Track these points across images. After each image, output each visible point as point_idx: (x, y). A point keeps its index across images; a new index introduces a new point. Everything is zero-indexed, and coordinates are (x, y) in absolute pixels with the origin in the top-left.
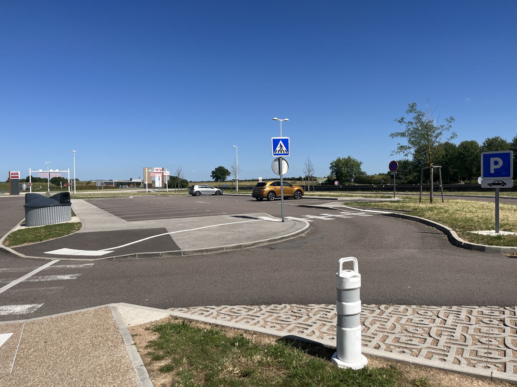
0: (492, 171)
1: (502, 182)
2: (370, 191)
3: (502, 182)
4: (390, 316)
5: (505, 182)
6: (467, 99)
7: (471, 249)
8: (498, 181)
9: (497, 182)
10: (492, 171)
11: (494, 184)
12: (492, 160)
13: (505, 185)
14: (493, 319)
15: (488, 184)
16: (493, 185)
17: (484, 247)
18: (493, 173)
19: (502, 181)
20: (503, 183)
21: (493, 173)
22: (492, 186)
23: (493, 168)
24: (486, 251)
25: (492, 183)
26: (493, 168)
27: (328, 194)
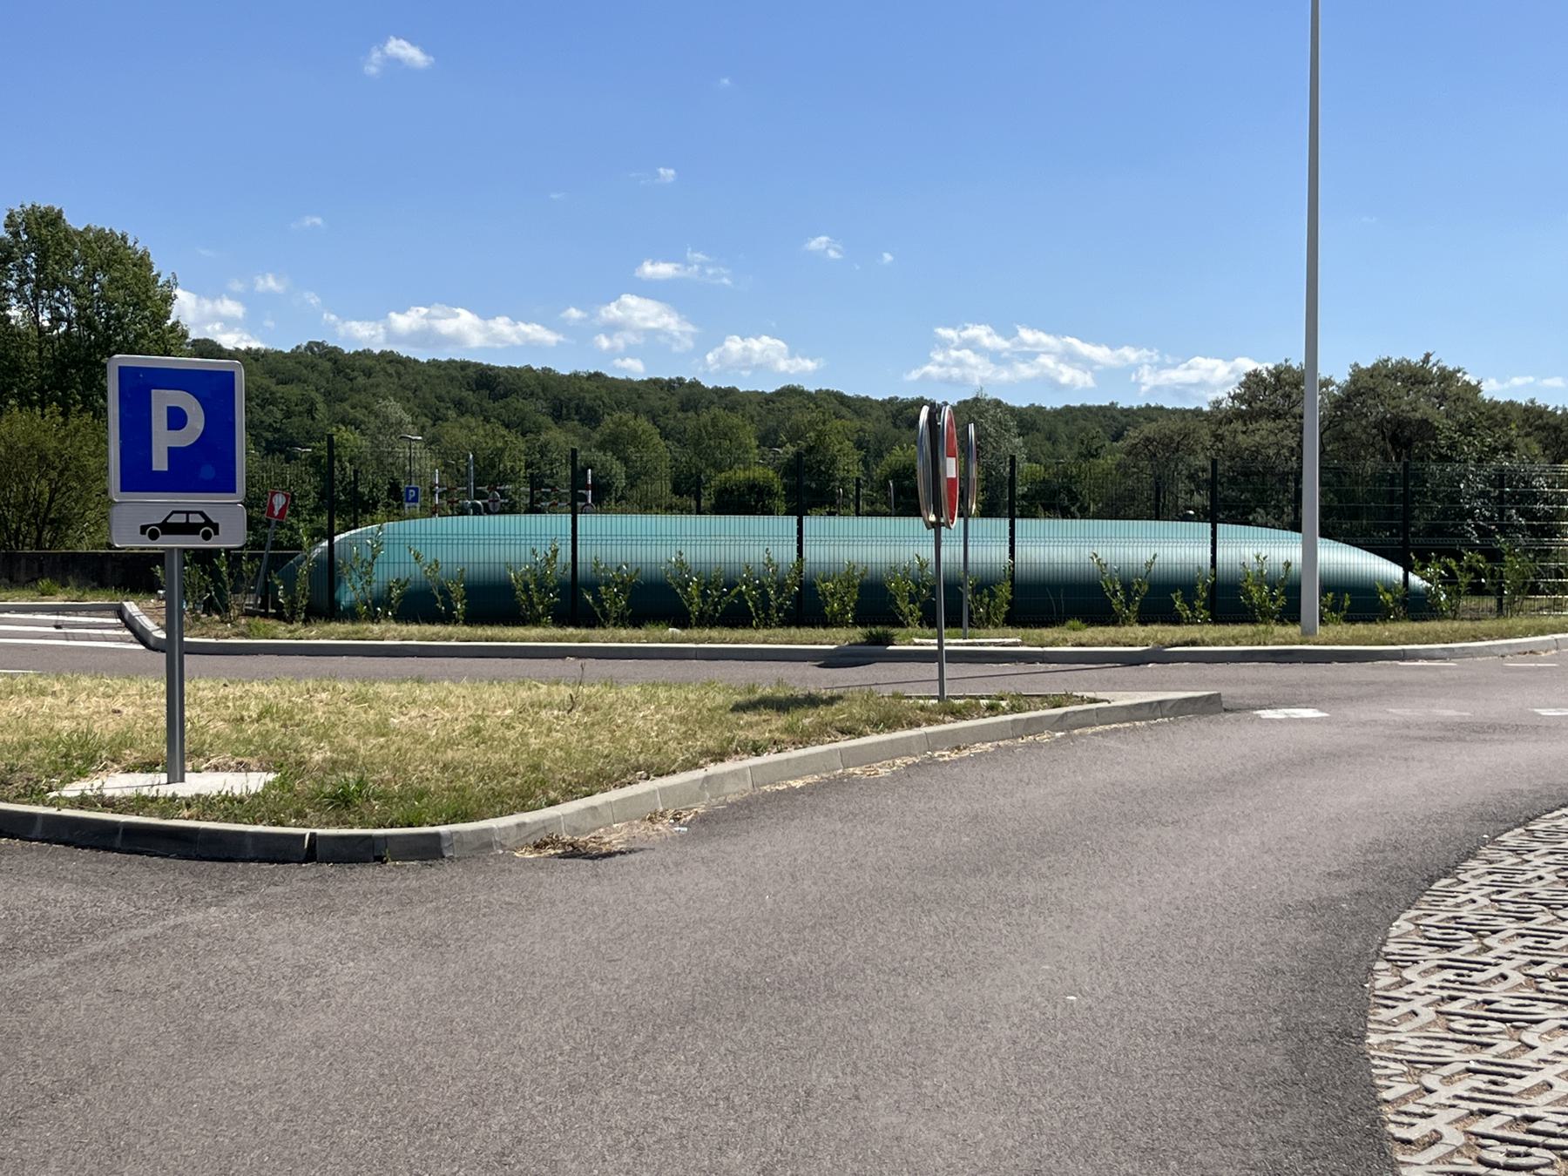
0: (160, 463)
1: (203, 521)
2: (44, 583)
3: (203, 521)
4: (1496, 977)
5: (214, 521)
6: (554, 196)
7: (380, 859)
8: (188, 513)
9: (181, 519)
10: (160, 463)
11: (168, 528)
12: (162, 401)
13: (217, 533)
14: (1454, 982)
15: (143, 529)
16: (163, 534)
17: (437, 836)
18: (166, 469)
19: (202, 514)
20: (208, 522)
21: (166, 469)
22: (161, 537)
23: (163, 442)
24: (448, 854)
25: (160, 521)
26: (163, 442)
27: (527, 633)
